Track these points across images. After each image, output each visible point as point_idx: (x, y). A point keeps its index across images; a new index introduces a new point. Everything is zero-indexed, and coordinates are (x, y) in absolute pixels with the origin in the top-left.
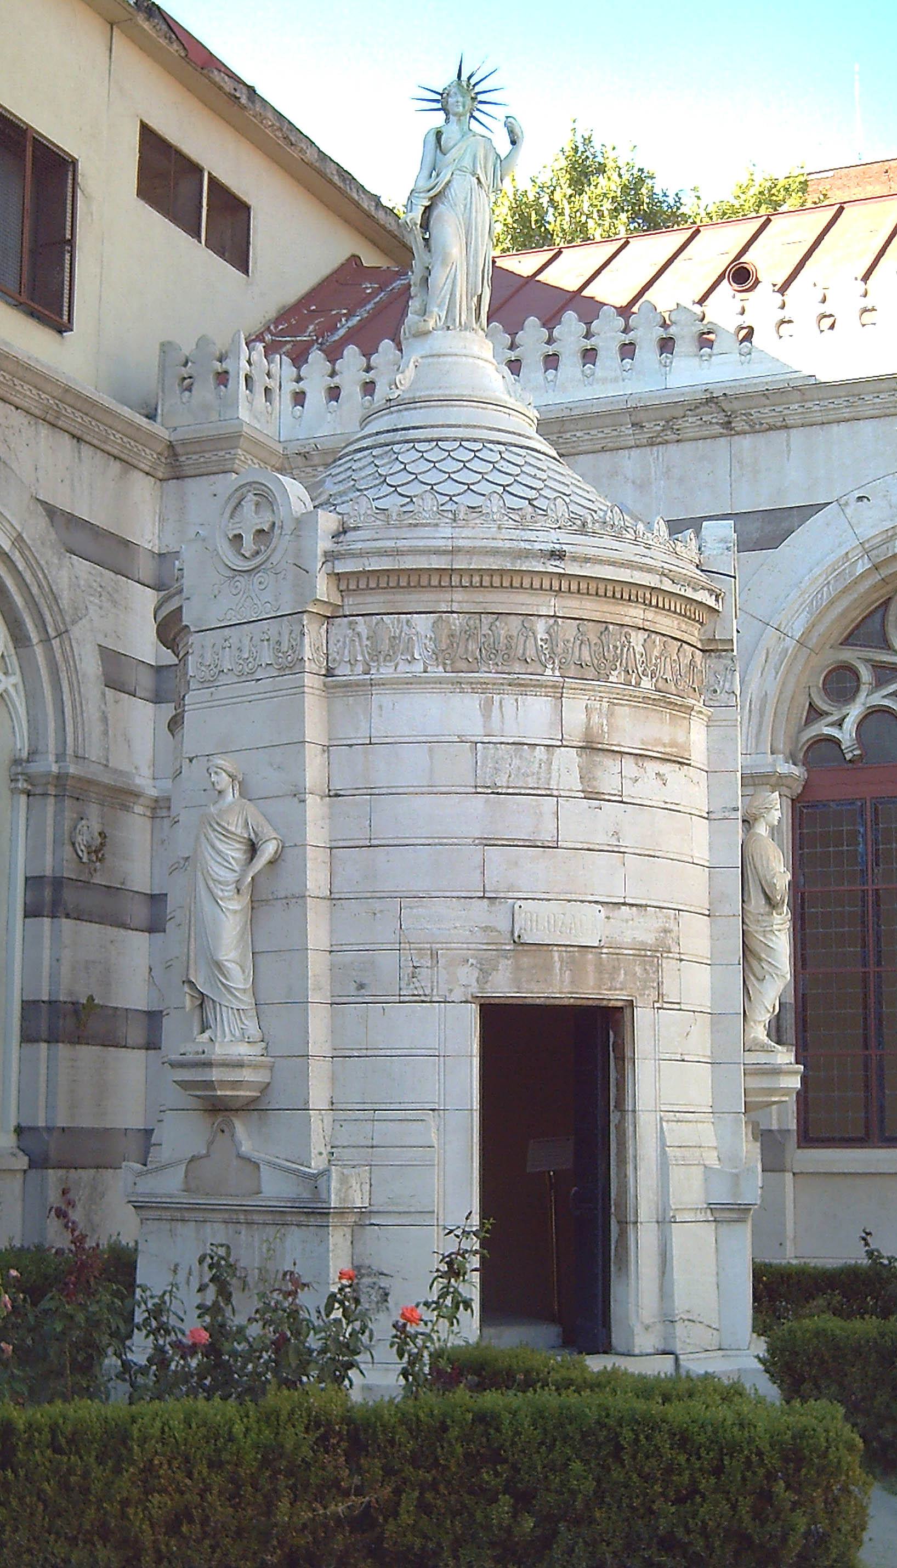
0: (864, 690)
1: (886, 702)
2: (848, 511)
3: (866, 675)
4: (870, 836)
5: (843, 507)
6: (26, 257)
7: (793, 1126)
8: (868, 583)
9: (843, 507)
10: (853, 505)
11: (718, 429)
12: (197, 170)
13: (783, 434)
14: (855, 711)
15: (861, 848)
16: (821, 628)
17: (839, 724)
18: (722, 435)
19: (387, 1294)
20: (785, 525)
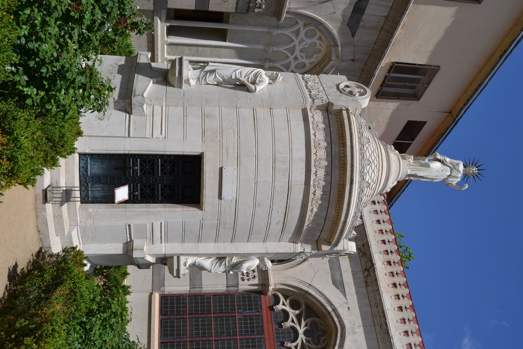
0: (294, 311)
1: (290, 318)
2: (345, 305)
3: (318, 36)
4: (251, 314)
5: (346, 303)
6: (329, 309)
7: (77, 183)
8: (324, 311)
9: (346, 303)
10: (347, 306)
11: (364, 267)
12: (413, 140)
13: (365, 286)
14: (288, 309)
15: (248, 311)
16: (311, 298)
17: (284, 304)
18: (363, 268)
19: (101, 120)
20: (339, 287)
